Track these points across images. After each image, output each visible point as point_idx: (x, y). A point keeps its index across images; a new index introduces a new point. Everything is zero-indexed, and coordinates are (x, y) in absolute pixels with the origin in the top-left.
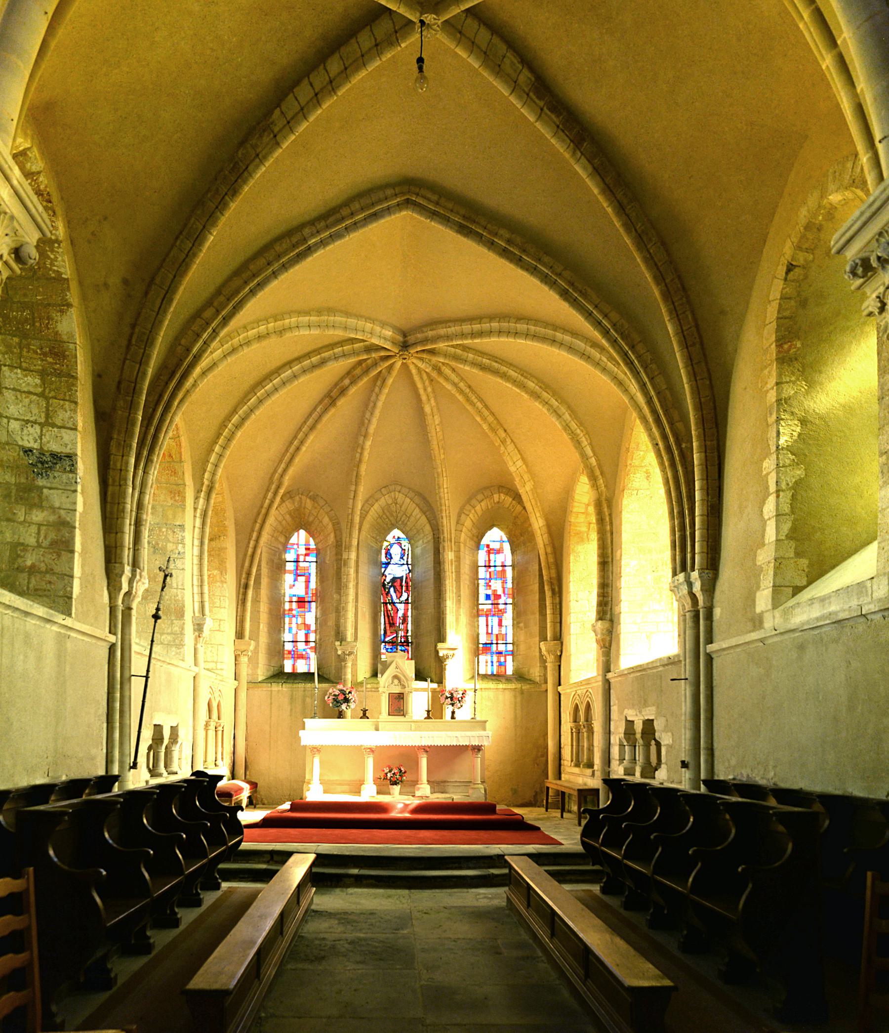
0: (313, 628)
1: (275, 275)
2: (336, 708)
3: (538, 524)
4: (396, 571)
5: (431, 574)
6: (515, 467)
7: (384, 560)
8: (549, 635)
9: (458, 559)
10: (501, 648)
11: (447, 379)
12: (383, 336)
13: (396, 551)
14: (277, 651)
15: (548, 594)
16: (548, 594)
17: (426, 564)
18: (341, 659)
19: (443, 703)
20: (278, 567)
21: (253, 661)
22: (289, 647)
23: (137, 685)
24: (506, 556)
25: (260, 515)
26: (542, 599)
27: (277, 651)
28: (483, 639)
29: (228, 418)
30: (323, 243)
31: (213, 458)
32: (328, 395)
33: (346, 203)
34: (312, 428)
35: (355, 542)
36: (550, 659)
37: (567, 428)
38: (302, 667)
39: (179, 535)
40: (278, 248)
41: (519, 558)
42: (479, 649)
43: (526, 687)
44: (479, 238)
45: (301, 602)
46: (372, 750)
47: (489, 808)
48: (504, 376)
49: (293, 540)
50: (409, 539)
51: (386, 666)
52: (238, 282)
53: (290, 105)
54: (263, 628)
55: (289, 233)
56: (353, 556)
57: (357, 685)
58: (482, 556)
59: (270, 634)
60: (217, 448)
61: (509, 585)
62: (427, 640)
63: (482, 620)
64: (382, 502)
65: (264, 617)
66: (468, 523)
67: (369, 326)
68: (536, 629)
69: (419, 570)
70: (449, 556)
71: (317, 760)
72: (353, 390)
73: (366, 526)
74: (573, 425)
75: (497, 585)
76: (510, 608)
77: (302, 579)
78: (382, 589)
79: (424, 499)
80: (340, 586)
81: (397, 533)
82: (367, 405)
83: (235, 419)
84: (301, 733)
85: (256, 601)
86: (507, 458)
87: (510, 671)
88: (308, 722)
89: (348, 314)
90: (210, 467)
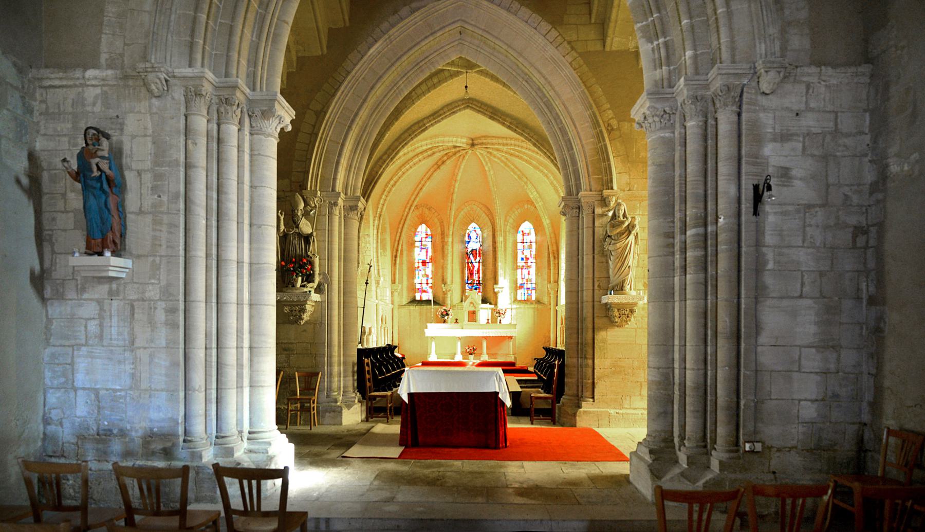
0: (430, 276)
1: (412, 139)
3: (546, 222)
4: (474, 245)
5: (491, 248)
6: (533, 195)
7: (467, 240)
8: (552, 280)
9: (505, 240)
10: (529, 286)
11: (495, 157)
12: (462, 142)
13: (473, 235)
14: (412, 289)
15: (552, 259)
16: (552, 259)
17: (489, 242)
18: (445, 293)
19: (497, 315)
20: (412, 245)
21: (401, 294)
23: (360, 311)
24: (532, 237)
25: (403, 220)
26: (549, 261)
28: (520, 281)
29: (389, 182)
30: (432, 125)
31: (382, 202)
32: (436, 164)
33: (442, 109)
34: (428, 179)
35: (451, 233)
36: (552, 292)
37: (552, 183)
38: (425, 297)
39: (367, 239)
40: (414, 128)
41: (539, 238)
42: (517, 287)
43: (540, 307)
44: (499, 122)
45: (424, 263)
46: (459, 338)
47: (513, 364)
48: (521, 158)
49: (419, 229)
50: (481, 229)
51: (467, 298)
52: (397, 143)
53: (419, 91)
54: (405, 277)
55: (418, 122)
56: (450, 240)
57: (453, 306)
58: (519, 237)
59: (408, 280)
60: (384, 197)
61: (534, 253)
62: (490, 283)
63: (519, 271)
64: (465, 210)
65: (405, 271)
66: (511, 221)
67: (455, 139)
68: (546, 277)
69: (486, 245)
70: (500, 239)
71: (433, 343)
72: (448, 162)
73: (457, 223)
74: (555, 182)
75: (527, 253)
76: (534, 265)
77: (424, 251)
78: (467, 255)
79: (488, 209)
81: (473, 225)
82: (456, 167)
83: (392, 182)
84: (426, 330)
85: (401, 264)
86: (528, 191)
87: (533, 298)
88: (429, 325)
89: (444, 136)
90: (380, 206)
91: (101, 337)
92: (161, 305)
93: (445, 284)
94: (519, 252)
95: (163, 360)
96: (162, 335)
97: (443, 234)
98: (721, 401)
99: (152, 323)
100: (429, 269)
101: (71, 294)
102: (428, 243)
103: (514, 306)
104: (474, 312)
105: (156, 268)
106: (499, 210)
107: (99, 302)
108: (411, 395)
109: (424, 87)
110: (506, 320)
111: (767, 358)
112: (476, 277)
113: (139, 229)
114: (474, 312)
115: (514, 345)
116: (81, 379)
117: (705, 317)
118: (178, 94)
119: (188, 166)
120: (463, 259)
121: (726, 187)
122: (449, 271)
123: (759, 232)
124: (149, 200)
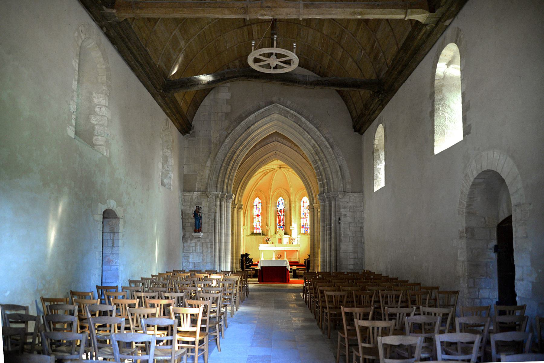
2: (267, 241)
4: (281, 207)
9: (295, 206)
13: (281, 203)
14: (252, 228)
17: (288, 206)
18: (267, 230)
19: (291, 240)
20: (252, 207)
21: (247, 231)
22: (255, 226)
27: (252, 228)
38: (258, 231)
45: (258, 216)
47: (297, 262)
51: (277, 232)
54: (249, 222)
57: (271, 236)
58: (302, 204)
63: (302, 220)
66: (298, 197)
69: (286, 208)
70: (293, 205)
77: (258, 210)
80: (267, 213)
81: (281, 198)
85: (247, 216)
91: (196, 251)
92: (209, 243)
93: (268, 226)
94: (302, 210)
95: (209, 256)
96: (209, 249)
97: (267, 203)
98: (333, 265)
99: (207, 247)
100: (260, 218)
101: (189, 241)
102: (260, 206)
103: (299, 236)
104: (281, 239)
105: (208, 235)
106: (292, 192)
107: (195, 243)
108: (261, 267)
109: (258, 147)
110: (295, 243)
111: (342, 255)
112: (282, 223)
113: (204, 227)
114: (281, 239)
115: (299, 254)
116: (191, 260)
117: (330, 246)
118: (214, 197)
119: (215, 213)
120: (276, 214)
121: (333, 218)
122: (270, 220)
123: (340, 228)
124: (207, 220)
